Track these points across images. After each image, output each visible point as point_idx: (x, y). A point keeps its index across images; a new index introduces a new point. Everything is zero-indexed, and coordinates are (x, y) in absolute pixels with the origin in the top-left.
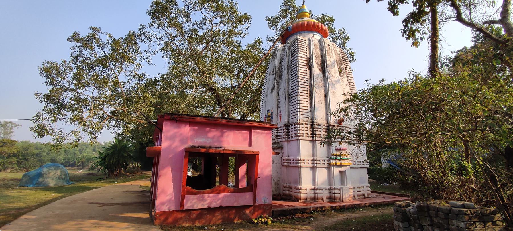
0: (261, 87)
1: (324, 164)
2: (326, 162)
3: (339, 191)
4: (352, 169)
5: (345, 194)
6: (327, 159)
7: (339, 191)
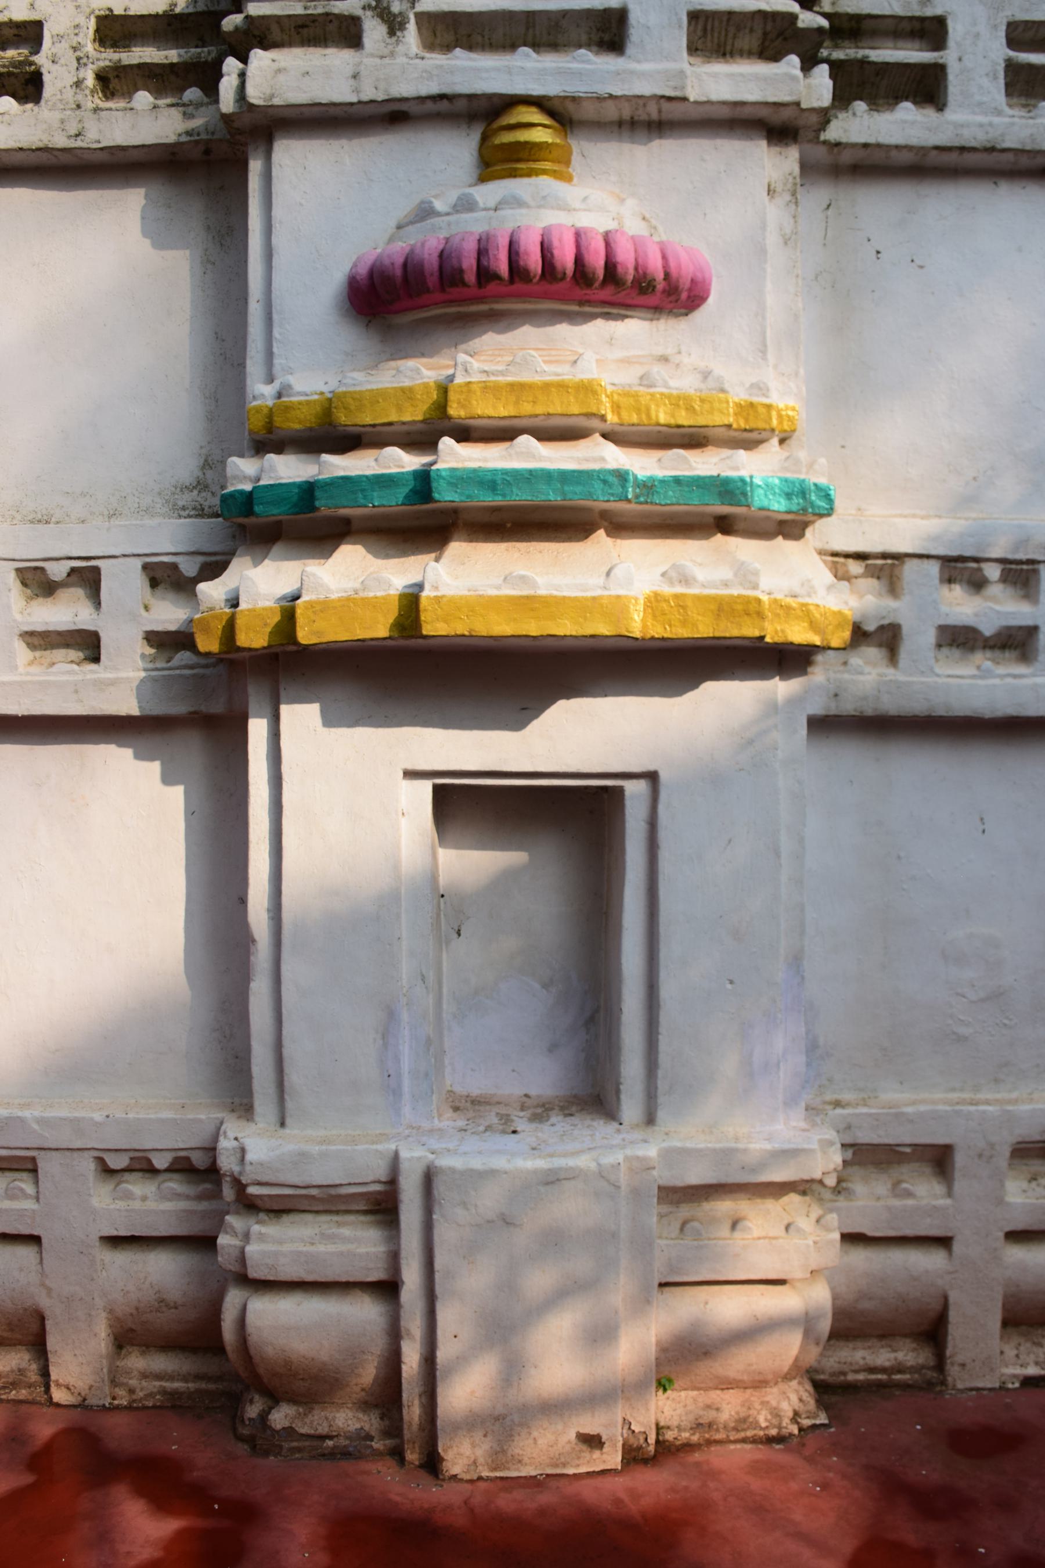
3: (355, 1246)
4: (854, 760)
5: (504, 1329)
6: (169, 537)
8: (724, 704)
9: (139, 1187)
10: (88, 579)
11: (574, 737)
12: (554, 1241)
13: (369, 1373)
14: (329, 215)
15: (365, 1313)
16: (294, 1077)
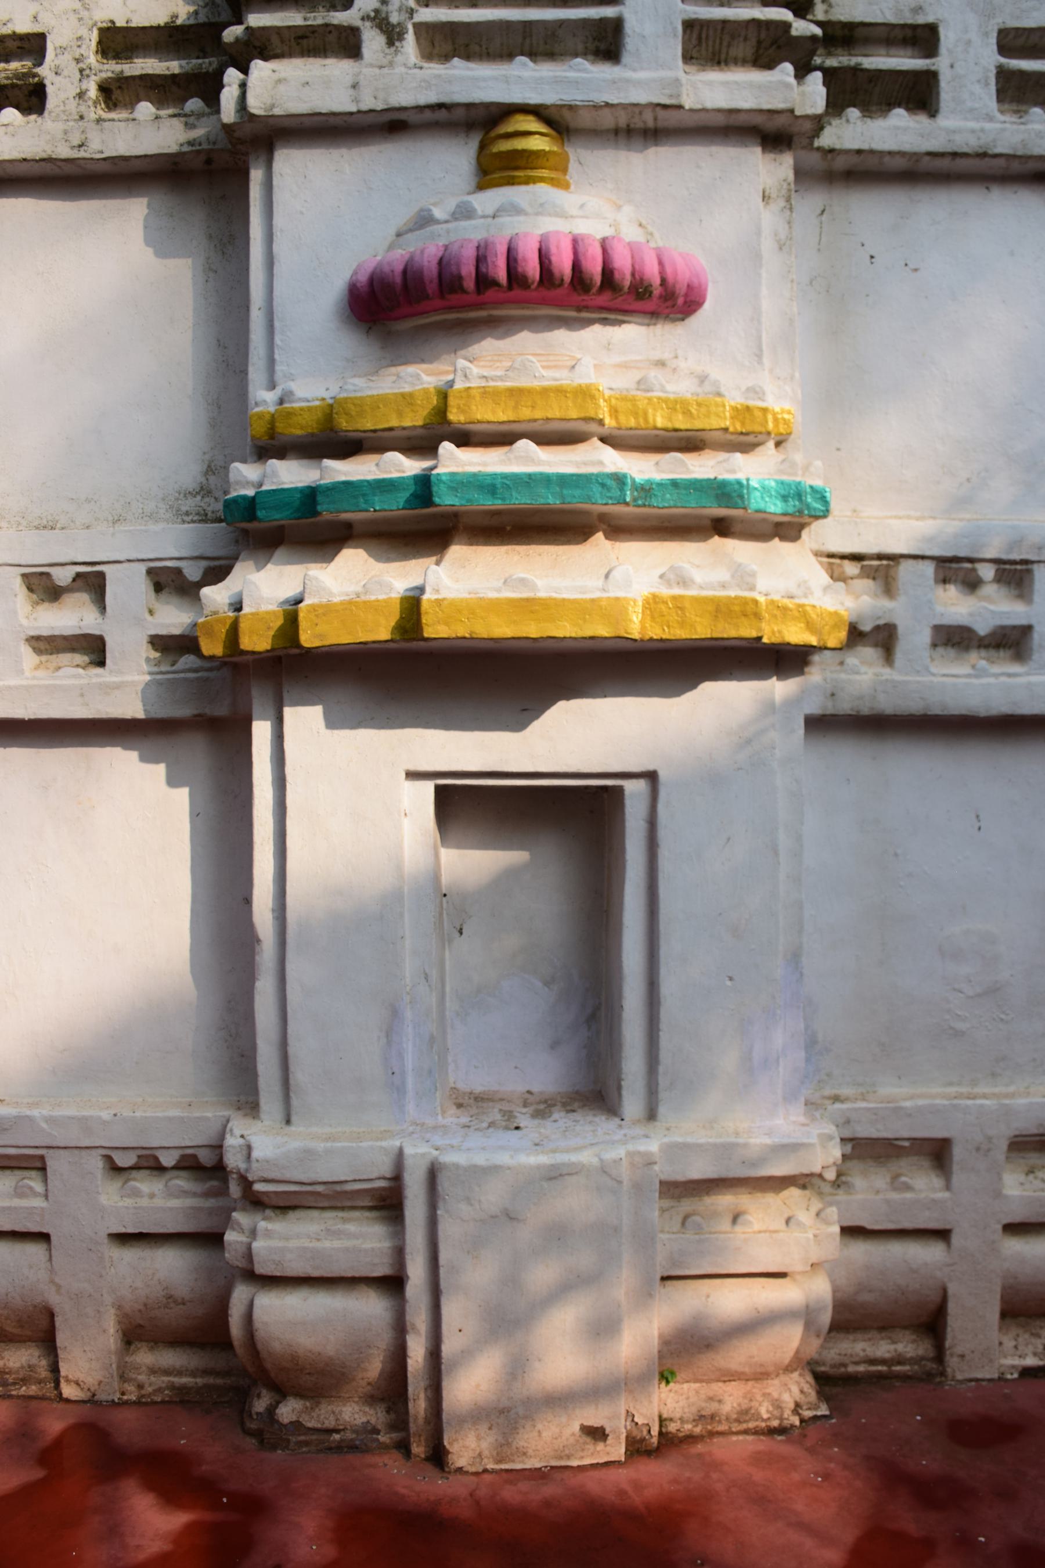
0: (852, 578)
1: (94, 649)
2: (136, 616)
3: (361, 1241)
4: (850, 759)
5: (509, 1320)
6: (174, 542)
7: (361, 1241)
8: (723, 704)
9: (147, 1185)
10: (93, 583)
11: (574, 737)
12: (557, 1236)
13: (375, 1367)
14: (326, 219)
15: (371, 1307)
16: (299, 1075)
